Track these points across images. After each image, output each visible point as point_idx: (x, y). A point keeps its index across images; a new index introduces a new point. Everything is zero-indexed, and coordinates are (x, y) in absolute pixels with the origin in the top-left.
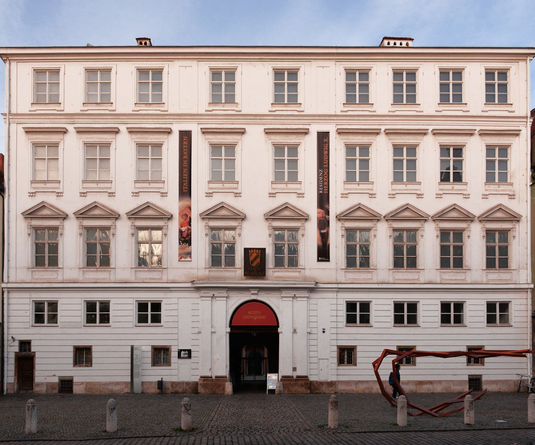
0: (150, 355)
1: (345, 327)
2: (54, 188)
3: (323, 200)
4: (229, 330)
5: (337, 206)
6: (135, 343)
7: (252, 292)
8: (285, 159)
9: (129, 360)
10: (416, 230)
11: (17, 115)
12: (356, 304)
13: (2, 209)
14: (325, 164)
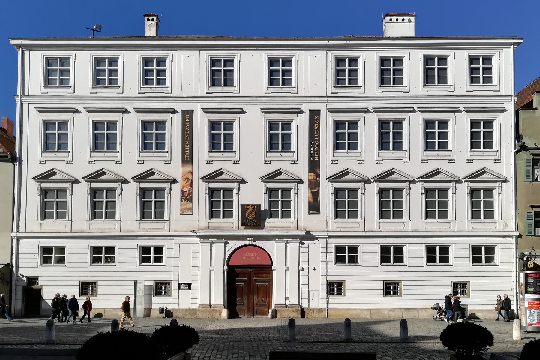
3: (314, 165)
5: (328, 169)
8: (278, 137)
13: (13, 174)
14: (317, 137)
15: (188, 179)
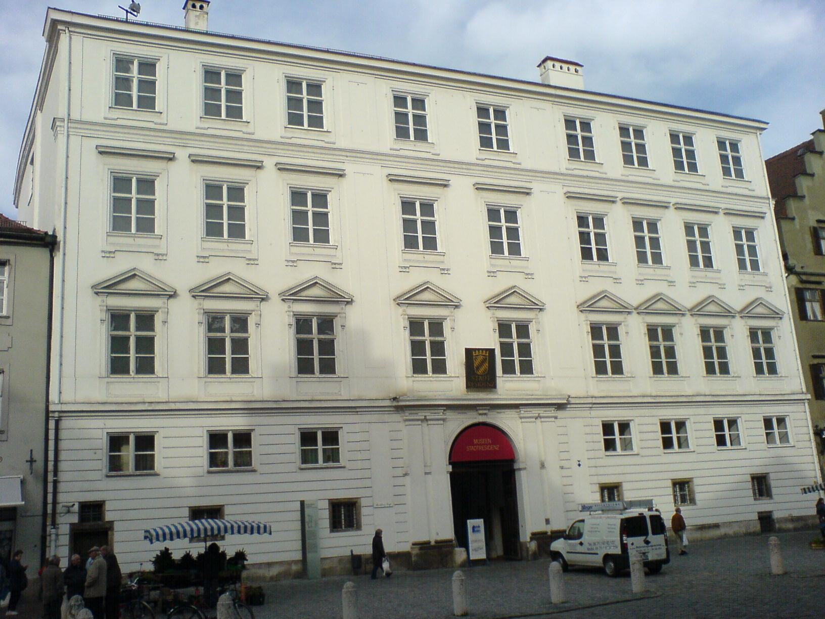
2: (521, 267)
4: (450, 468)
6: (307, 497)
7: (481, 412)
9: (298, 525)
11: (80, 122)
12: (316, 433)
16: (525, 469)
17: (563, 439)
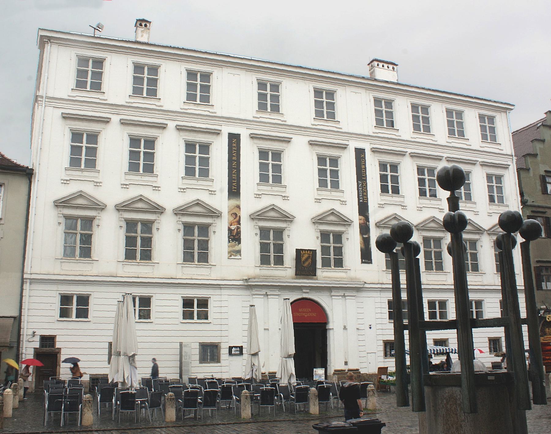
0: (197, 351)
1: (388, 323)
3: (363, 208)
5: (375, 215)
7: (304, 291)
10: (152, 222)
14: (364, 177)
15: (236, 214)
16: (333, 329)
17: (360, 311)
